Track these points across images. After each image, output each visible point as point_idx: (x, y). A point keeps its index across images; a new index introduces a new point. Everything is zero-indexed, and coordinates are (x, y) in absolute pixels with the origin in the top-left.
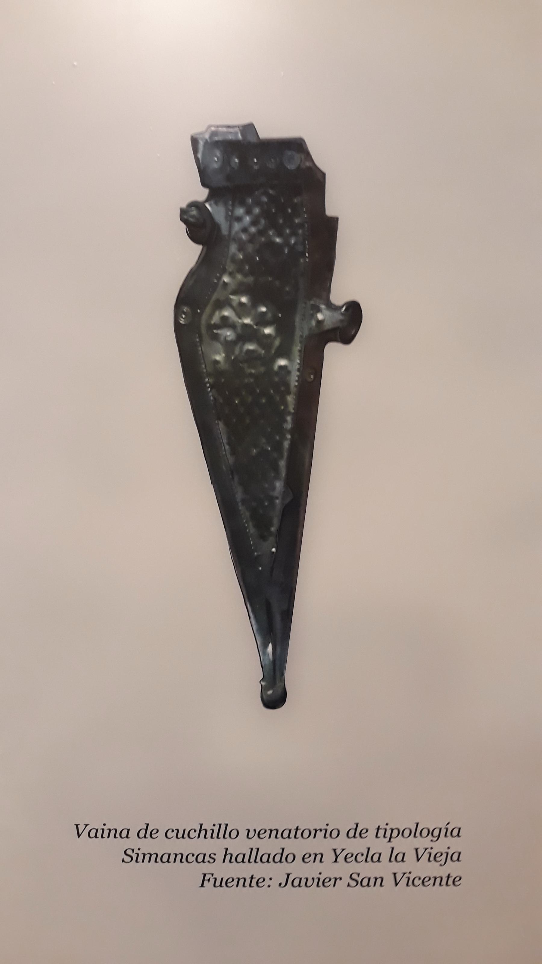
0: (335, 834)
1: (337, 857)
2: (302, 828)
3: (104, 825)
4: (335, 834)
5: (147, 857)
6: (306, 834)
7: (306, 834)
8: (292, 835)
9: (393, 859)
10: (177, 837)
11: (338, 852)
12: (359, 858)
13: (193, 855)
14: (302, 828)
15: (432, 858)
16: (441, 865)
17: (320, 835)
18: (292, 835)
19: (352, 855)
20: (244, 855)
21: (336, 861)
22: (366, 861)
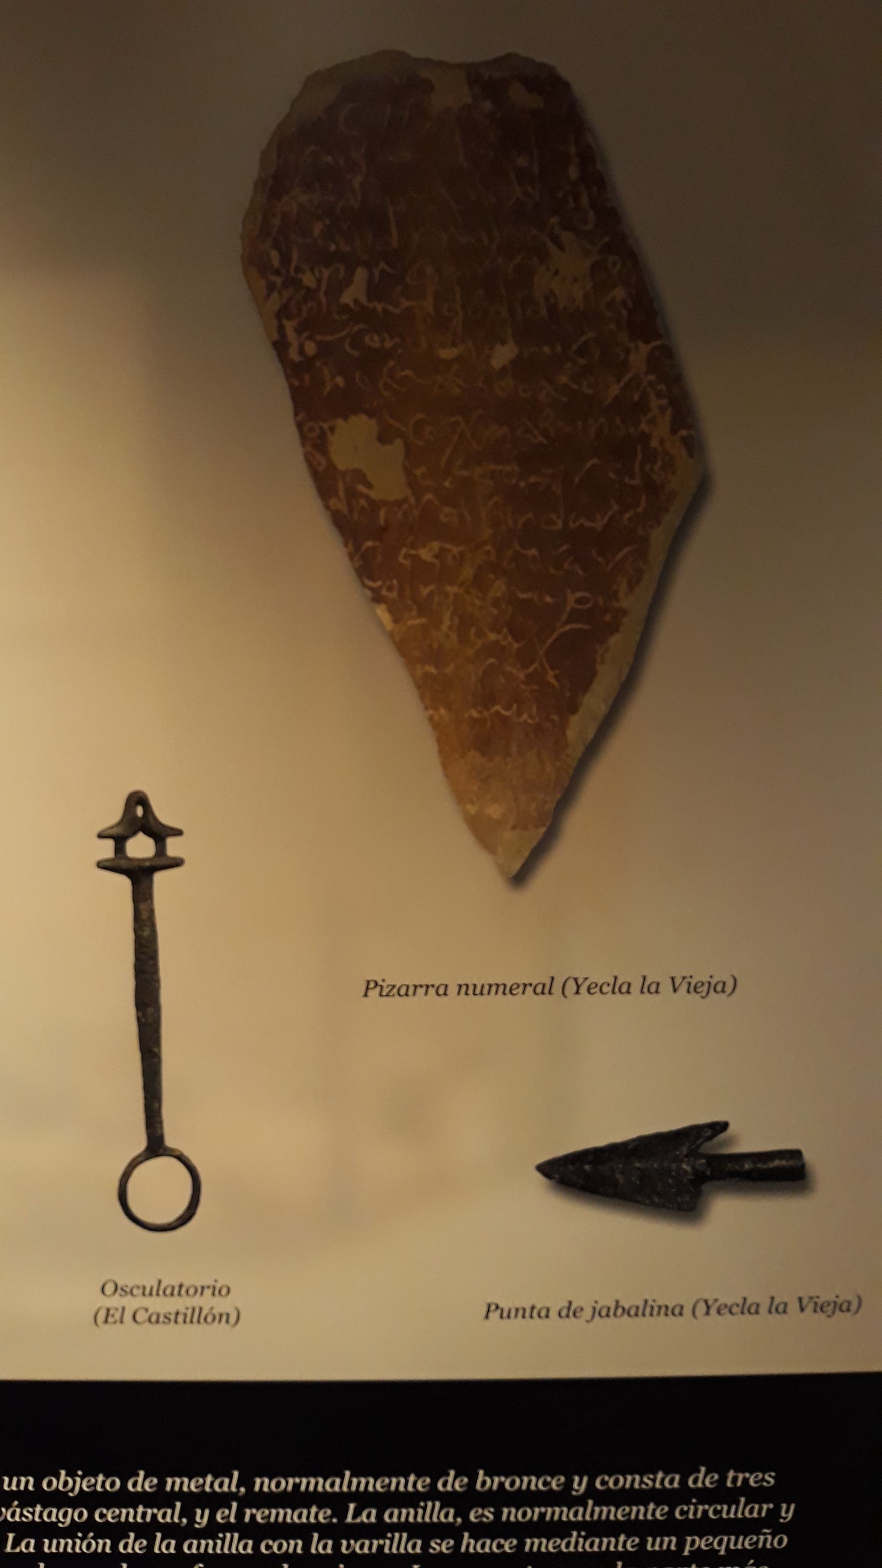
0: (224, 1292)
1: (578, 987)
2: (538, 1306)
3: (837, 1297)
4: (224, 1292)
5: (494, 989)
6: (192, 1291)
7: (192, 1291)
8: (176, 1292)
9: (645, 990)
10: (144, 1294)
11: (580, 982)
12: (605, 989)
13: (608, 985)
14: (538, 1306)
15: (692, 989)
16: (703, 997)
17: (208, 1292)
18: (176, 1292)
19: (596, 986)
20: (544, 985)
21: (577, 993)
22: (613, 992)
